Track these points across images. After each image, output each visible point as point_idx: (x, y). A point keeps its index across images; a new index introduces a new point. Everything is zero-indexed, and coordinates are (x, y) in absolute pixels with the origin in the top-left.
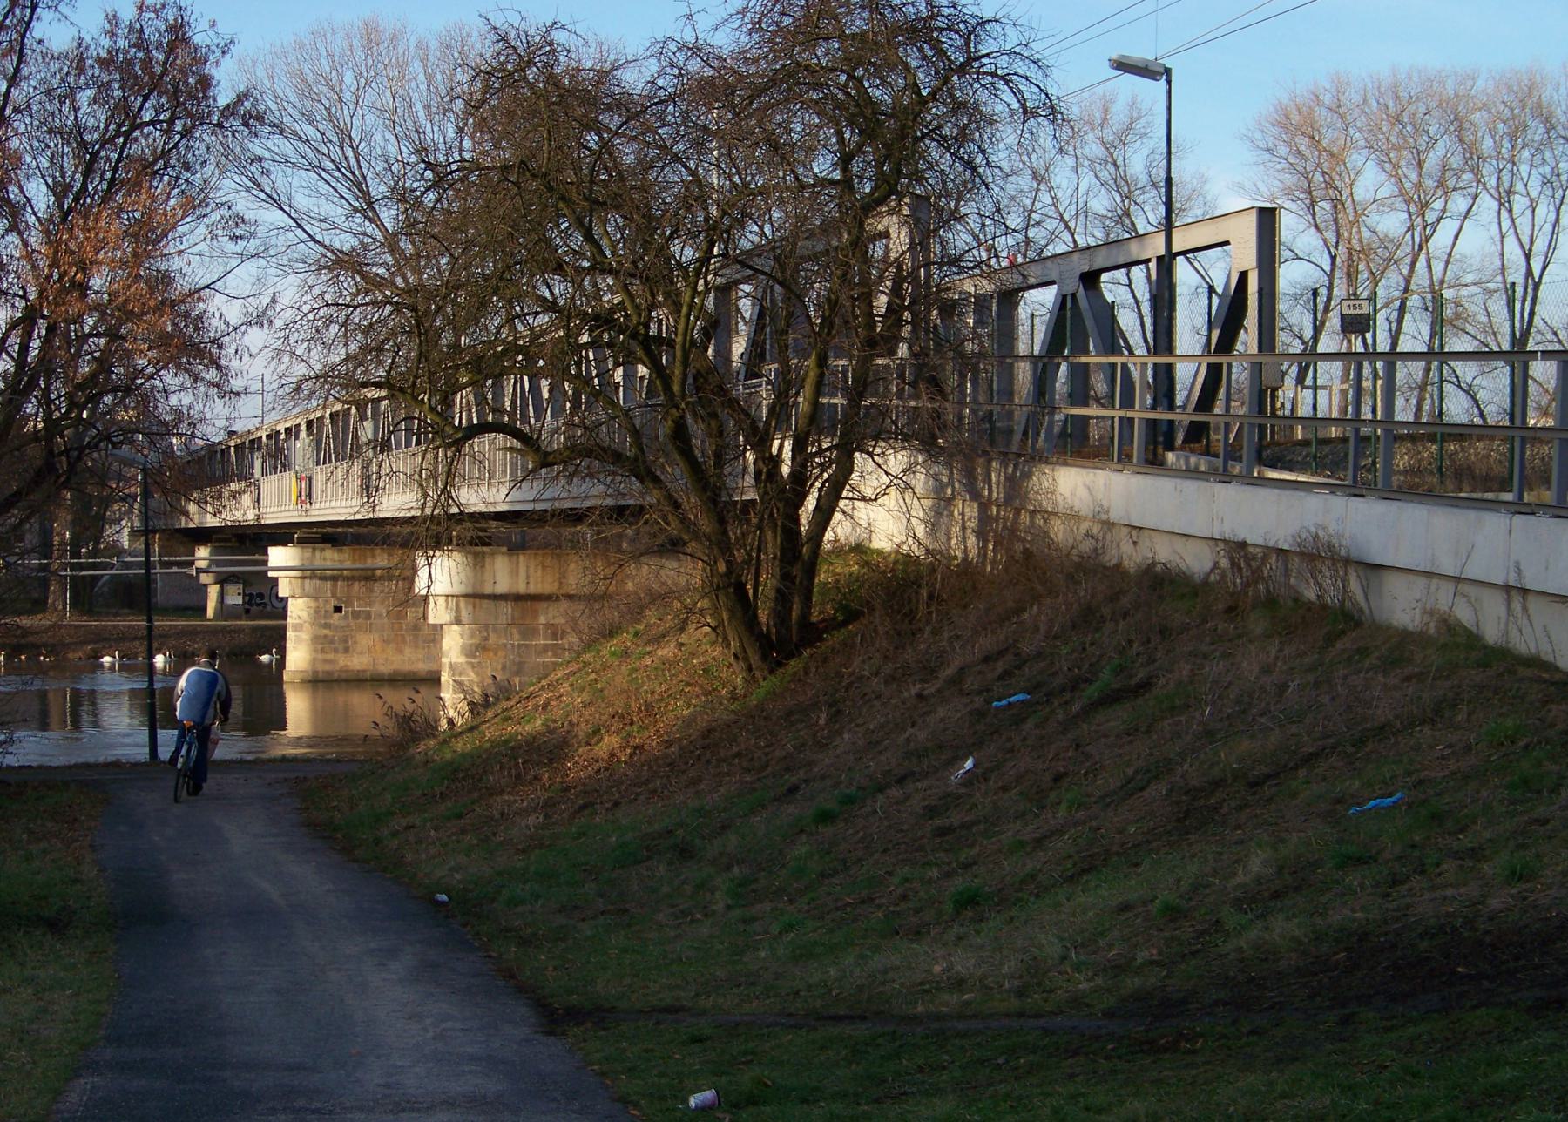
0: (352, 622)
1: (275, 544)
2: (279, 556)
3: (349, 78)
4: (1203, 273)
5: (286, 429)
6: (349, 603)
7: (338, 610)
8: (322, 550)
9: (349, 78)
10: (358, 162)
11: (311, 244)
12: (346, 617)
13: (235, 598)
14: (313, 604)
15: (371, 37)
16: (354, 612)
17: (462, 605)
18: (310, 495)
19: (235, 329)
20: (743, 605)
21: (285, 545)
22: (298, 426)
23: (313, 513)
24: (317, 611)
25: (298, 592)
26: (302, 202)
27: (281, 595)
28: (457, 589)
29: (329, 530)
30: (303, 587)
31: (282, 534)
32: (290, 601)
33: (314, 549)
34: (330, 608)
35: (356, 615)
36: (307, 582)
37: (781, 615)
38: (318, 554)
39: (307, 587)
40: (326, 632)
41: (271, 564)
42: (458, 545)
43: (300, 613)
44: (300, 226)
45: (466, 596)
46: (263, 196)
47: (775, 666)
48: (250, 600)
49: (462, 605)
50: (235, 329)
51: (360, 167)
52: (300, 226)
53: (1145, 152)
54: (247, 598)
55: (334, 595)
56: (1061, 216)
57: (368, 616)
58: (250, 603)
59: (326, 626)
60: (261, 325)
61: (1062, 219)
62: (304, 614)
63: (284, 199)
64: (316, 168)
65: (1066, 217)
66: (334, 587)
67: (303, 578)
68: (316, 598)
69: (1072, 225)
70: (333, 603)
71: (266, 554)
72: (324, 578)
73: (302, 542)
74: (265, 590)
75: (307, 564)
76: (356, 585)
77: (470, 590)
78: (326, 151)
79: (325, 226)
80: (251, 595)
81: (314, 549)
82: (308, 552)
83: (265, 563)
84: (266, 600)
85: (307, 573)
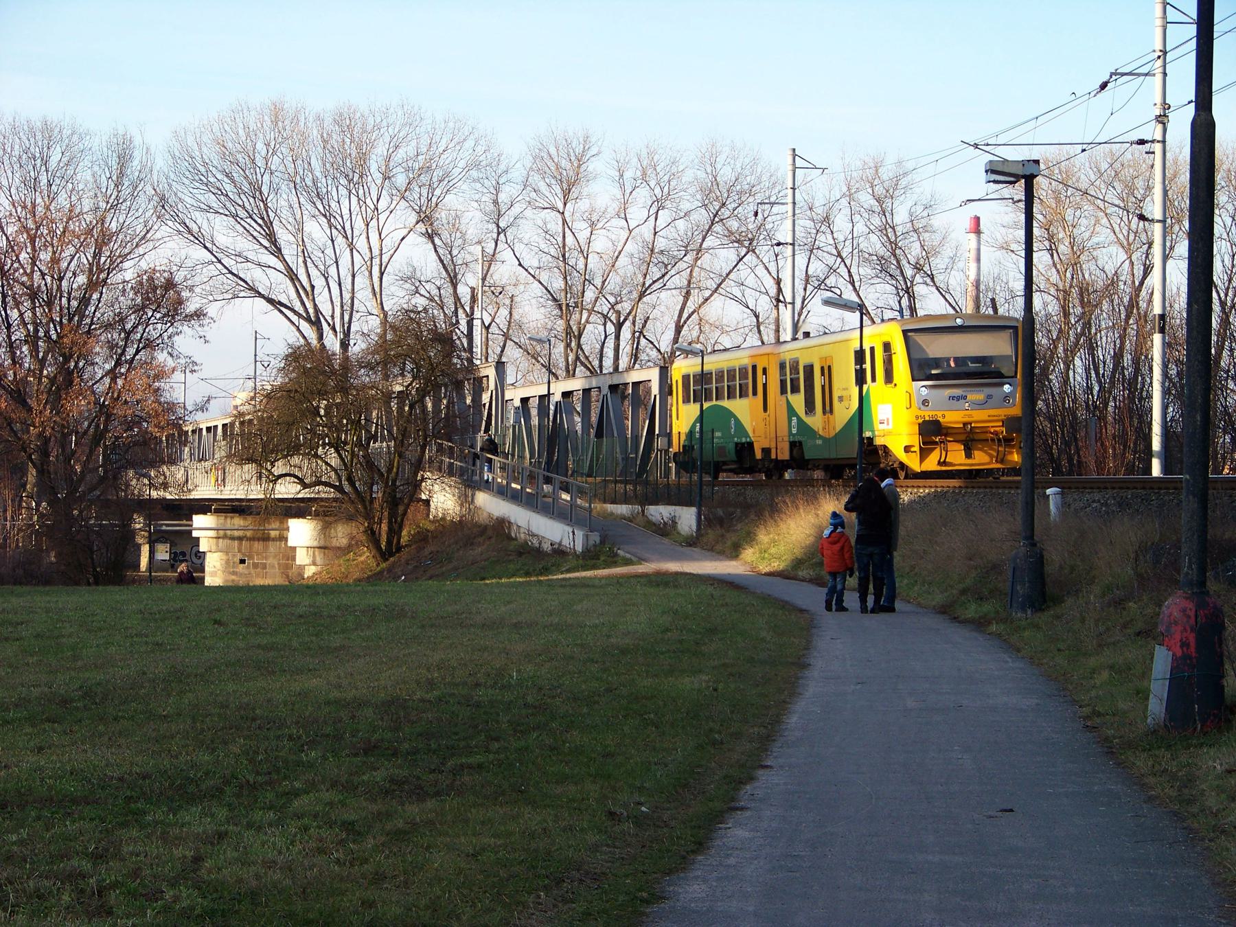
0: (252, 571)
1: (197, 513)
2: (199, 520)
3: (260, 146)
4: (954, 304)
5: (207, 428)
6: (251, 557)
7: (242, 561)
8: (232, 518)
9: (260, 146)
10: (267, 212)
11: (229, 276)
12: (248, 567)
13: (163, 553)
14: (224, 557)
15: (277, 114)
16: (254, 563)
17: (317, 553)
18: (224, 480)
19: (191, 412)
20: (376, 543)
21: (205, 513)
22: (216, 427)
23: (226, 492)
24: (227, 562)
25: (214, 548)
26: (222, 240)
27: (201, 550)
28: (315, 544)
29: (237, 503)
30: (217, 544)
31: (203, 506)
32: (208, 555)
33: (226, 517)
34: (237, 560)
35: (255, 566)
36: (221, 540)
37: (389, 542)
38: (229, 520)
39: (220, 545)
40: (234, 577)
41: (195, 525)
42: (315, 516)
43: (216, 564)
44: (220, 261)
45: (318, 548)
46: (192, 238)
47: (386, 560)
48: (175, 557)
49: (317, 553)
50: (191, 412)
51: (268, 216)
52: (220, 261)
53: (910, 203)
54: (173, 555)
55: (239, 551)
56: (839, 253)
57: (264, 566)
58: (174, 559)
59: (234, 573)
60: (203, 412)
61: (839, 255)
62: (218, 565)
63: (207, 236)
64: (235, 216)
65: (844, 255)
66: (240, 545)
67: (218, 538)
68: (227, 553)
69: (848, 262)
70: (239, 556)
71: (191, 520)
72: (233, 538)
73: (217, 511)
74: (187, 549)
75: (220, 527)
76: (256, 544)
77: (322, 543)
78: (241, 203)
79: (239, 259)
80: (175, 553)
81: (226, 517)
82: (222, 519)
83: (192, 526)
84: (187, 557)
85: (222, 534)
